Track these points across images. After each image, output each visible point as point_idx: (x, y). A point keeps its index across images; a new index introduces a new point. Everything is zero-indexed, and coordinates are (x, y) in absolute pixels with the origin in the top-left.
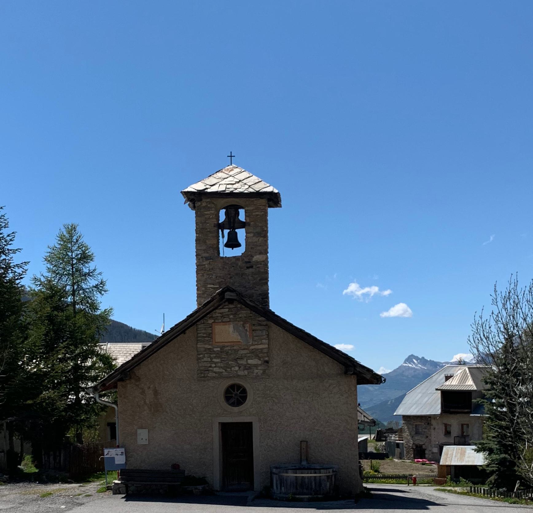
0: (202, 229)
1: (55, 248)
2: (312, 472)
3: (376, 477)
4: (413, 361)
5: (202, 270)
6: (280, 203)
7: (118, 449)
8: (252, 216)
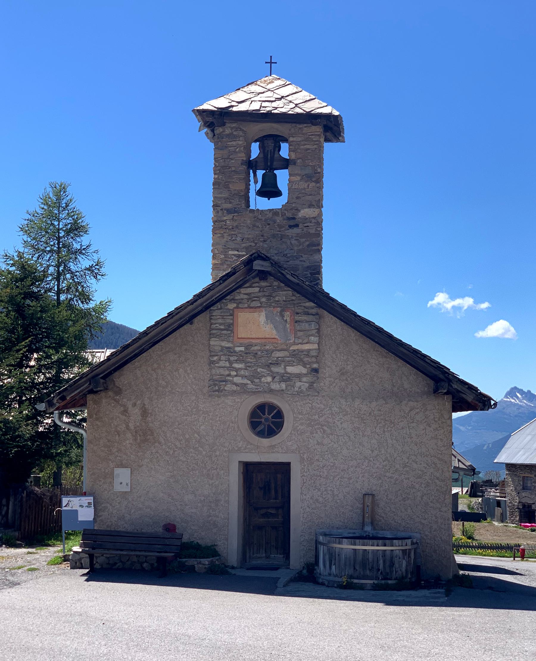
0: (222, 167)
1: (36, 215)
2: (380, 544)
3: (470, 547)
4: (517, 395)
5: (221, 228)
6: (342, 134)
7: (83, 498)
8: (299, 151)
